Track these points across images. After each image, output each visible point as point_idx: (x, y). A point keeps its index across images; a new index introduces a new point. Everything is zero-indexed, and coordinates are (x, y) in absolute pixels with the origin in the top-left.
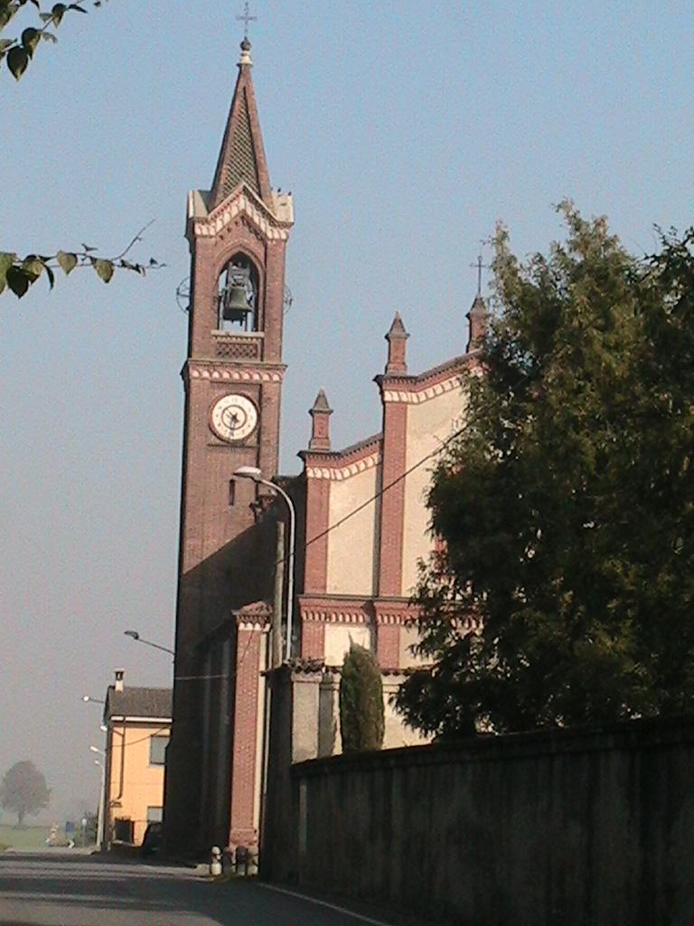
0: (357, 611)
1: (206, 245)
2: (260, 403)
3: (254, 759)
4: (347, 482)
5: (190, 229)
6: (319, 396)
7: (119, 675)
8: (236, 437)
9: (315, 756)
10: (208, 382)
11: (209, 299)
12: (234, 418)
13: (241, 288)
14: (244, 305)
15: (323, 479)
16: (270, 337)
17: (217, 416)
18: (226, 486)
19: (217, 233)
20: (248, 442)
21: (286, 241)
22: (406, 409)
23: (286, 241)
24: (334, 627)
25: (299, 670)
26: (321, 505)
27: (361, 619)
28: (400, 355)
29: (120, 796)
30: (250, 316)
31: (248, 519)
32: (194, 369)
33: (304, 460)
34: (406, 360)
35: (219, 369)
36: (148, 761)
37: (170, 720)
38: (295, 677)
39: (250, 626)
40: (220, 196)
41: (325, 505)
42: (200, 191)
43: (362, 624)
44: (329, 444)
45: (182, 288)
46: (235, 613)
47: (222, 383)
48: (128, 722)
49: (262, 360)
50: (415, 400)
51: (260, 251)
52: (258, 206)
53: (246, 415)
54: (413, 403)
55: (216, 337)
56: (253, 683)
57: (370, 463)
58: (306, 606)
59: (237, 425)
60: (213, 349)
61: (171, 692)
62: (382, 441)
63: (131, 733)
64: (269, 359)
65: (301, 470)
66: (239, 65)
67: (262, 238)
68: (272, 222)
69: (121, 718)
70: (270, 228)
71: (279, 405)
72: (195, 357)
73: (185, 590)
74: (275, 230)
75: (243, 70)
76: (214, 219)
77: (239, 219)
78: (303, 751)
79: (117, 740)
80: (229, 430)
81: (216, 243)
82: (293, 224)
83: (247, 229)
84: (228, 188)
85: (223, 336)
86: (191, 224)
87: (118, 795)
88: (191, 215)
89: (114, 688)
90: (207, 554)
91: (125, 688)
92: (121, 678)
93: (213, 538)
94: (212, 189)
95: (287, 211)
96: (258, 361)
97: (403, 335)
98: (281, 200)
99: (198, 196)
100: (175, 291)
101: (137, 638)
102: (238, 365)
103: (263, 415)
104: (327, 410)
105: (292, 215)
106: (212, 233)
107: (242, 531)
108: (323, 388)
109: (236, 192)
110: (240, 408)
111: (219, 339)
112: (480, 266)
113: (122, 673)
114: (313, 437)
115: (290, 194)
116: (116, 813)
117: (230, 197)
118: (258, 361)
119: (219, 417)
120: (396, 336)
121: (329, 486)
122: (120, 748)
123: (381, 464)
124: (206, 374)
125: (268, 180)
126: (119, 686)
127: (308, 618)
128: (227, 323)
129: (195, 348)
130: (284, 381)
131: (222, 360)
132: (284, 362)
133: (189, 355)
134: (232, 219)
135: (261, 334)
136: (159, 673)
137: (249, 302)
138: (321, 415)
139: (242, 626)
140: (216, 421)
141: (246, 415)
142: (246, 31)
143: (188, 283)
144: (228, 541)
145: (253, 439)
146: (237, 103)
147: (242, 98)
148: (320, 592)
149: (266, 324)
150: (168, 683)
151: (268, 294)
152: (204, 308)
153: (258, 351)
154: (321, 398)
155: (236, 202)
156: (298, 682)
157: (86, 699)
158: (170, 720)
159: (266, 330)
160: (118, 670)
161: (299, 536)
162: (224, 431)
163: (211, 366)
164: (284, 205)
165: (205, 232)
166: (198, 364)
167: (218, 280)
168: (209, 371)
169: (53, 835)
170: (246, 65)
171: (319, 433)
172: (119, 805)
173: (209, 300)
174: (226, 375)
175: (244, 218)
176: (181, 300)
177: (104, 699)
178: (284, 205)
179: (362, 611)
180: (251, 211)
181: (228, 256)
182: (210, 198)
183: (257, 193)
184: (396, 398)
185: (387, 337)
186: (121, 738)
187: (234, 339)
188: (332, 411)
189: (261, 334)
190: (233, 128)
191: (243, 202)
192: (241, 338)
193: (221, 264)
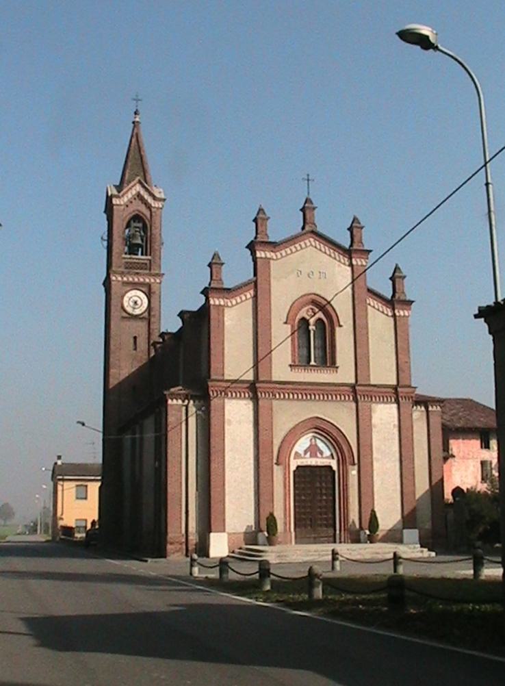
0: (244, 390)
2: (150, 294)
4: (279, 261)
5: (109, 202)
6: (215, 255)
10: (120, 283)
12: (136, 303)
18: (132, 341)
21: (161, 208)
22: (269, 263)
24: (230, 401)
26: (219, 321)
27: (247, 395)
29: (62, 514)
34: (268, 232)
36: (74, 498)
39: (175, 401)
40: (125, 185)
41: (221, 321)
42: (114, 186)
43: (247, 398)
44: (223, 284)
46: (165, 392)
47: (128, 283)
49: (150, 270)
50: (275, 258)
51: (147, 213)
52: (147, 190)
57: (249, 296)
58: (212, 387)
59: (137, 307)
60: (123, 266)
62: (256, 283)
63: (66, 484)
64: (154, 269)
65: (203, 302)
66: (134, 122)
67: (149, 207)
68: (154, 198)
69: (61, 477)
77: (136, 197)
79: (60, 488)
81: (124, 209)
83: (140, 202)
86: (109, 199)
88: (110, 194)
89: (56, 463)
90: (122, 378)
93: (124, 369)
96: (147, 272)
101: (83, 424)
102: (137, 273)
106: (122, 203)
107: (140, 365)
110: (139, 297)
112: (308, 180)
116: (61, 523)
120: (259, 220)
121: (223, 310)
123: (255, 297)
124: (120, 279)
126: (59, 462)
127: (213, 394)
130: (162, 283)
132: (162, 272)
134: (129, 200)
135: (149, 257)
138: (217, 265)
139: (170, 402)
140: (126, 304)
142: (137, 106)
144: (133, 370)
145: (146, 315)
147: (135, 137)
148: (221, 378)
152: (118, 245)
154: (216, 256)
155: (134, 188)
157: (44, 469)
162: (129, 310)
163: (122, 274)
165: (118, 203)
170: (138, 122)
172: (62, 519)
173: (121, 240)
174: (131, 279)
175: (139, 195)
177: (52, 469)
179: (247, 390)
180: (143, 192)
182: (119, 188)
183: (144, 183)
184: (263, 256)
188: (269, 218)
189: (149, 257)
191: (138, 188)
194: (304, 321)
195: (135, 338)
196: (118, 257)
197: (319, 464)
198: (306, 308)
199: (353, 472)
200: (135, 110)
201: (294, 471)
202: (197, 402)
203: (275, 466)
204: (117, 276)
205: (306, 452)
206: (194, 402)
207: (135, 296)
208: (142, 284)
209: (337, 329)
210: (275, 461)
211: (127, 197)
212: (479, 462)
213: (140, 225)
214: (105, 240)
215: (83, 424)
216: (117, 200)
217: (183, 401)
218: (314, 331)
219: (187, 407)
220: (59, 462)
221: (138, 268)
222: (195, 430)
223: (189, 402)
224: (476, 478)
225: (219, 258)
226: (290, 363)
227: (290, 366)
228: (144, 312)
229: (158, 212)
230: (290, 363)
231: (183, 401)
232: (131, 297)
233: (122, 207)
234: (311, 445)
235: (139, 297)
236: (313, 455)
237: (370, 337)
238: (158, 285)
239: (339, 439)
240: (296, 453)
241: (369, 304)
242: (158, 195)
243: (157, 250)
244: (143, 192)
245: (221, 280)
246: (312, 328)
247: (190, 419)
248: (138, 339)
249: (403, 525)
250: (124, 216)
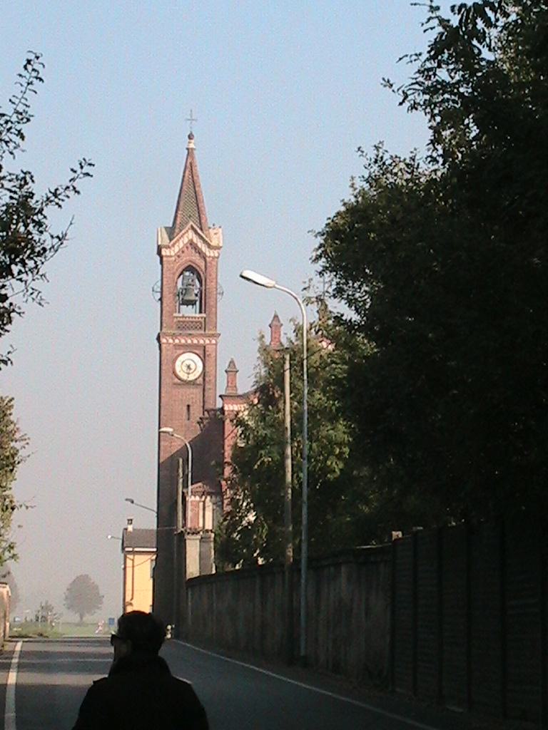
1: (169, 261)
2: (205, 357)
6: (231, 362)
7: (130, 521)
8: (189, 379)
9: (198, 575)
10: (171, 346)
11: (171, 295)
12: (189, 367)
13: (191, 287)
14: (193, 297)
16: (209, 317)
18: (185, 408)
19: (175, 254)
20: (198, 382)
21: (218, 258)
23: (218, 258)
25: (189, 533)
28: (278, 337)
29: (132, 599)
30: (198, 303)
31: (197, 431)
32: (163, 337)
33: (222, 399)
35: (179, 337)
38: (187, 537)
40: (177, 231)
45: (155, 287)
48: (137, 552)
49: (205, 330)
51: (202, 264)
52: (201, 237)
53: (196, 364)
55: (177, 317)
59: (192, 371)
60: (175, 326)
61: (155, 532)
64: (210, 330)
66: (188, 149)
67: (204, 258)
68: (209, 246)
69: (131, 549)
70: (207, 249)
71: (216, 360)
72: (164, 330)
74: (211, 251)
75: (190, 152)
76: (173, 245)
77: (188, 245)
78: (192, 573)
79: (129, 563)
80: (186, 375)
81: (175, 261)
82: (221, 247)
83: (193, 251)
84: (182, 226)
85: (180, 317)
87: (130, 597)
89: (126, 529)
91: (134, 529)
92: (131, 523)
94: (173, 225)
95: (219, 238)
97: (279, 324)
98: (215, 231)
99: (164, 230)
100: (151, 290)
101: (132, 502)
103: (206, 365)
104: (235, 370)
105: (221, 242)
106: (173, 254)
108: (232, 357)
109: (187, 229)
110: (193, 361)
111: (179, 319)
113: (131, 520)
114: (228, 386)
115: (220, 227)
117: (183, 232)
118: (203, 332)
122: (131, 569)
124: (171, 341)
125: (206, 220)
126: (130, 528)
128: (183, 307)
129: (164, 325)
131: (181, 332)
133: (161, 330)
135: (204, 315)
136: (148, 521)
137: (196, 295)
140: (178, 369)
141: (196, 364)
143: (159, 284)
145: (201, 379)
146: (187, 172)
147: (190, 168)
149: (207, 309)
150: (154, 527)
151: (207, 290)
153: (202, 326)
155: (187, 234)
156: (189, 539)
157: (109, 537)
158: (155, 550)
159: (207, 312)
160: (129, 518)
162: (184, 376)
163: (174, 336)
164: (216, 234)
165: (168, 254)
166: (166, 335)
167: (176, 283)
168: (172, 338)
169: (100, 628)
170: (192, 149)
171: (231, 383)
172: (131, 604)
174: (183, 341)
175: (191, 243)
176: (155, 294)
177: (121, 537)
178: (216, 234)
180: (196, 240)
181: (183, 267)
182: (171, 232)
183: (201, 226)
185: (270, 326)
186: (131, 562)
187: (187, 319)
190: (184, 188)
191: (191, 235)
192: (192, 318)
193: (180, 270)
195: (188, 406)
196: (169, 316)
200: (189, 133)
202: (214, 498)
204: (168, 338)
206: (211, 497)
207: (189, 359)
208: (197, 346)
211: (178, 246)
214: (157, 292)
215: (132, 502)
216: (168, 251)
217: (201, 497)
219: (204, 502)
220: (130, 528)
222: (211, 518)
223: (206, 498)
225: (234, 365)
228: (199, 377)
229: (214, 263)
231: (201, 497)
232: (184, 362)
233: (173, 259)
235: (193, 361)
238: (214, 346)
242: (214, 243)
243: (212, 306)
244: (196, 240)
245: (235, 386)
247: (207, 509)
248: (191, 408)
250: (176, 268)
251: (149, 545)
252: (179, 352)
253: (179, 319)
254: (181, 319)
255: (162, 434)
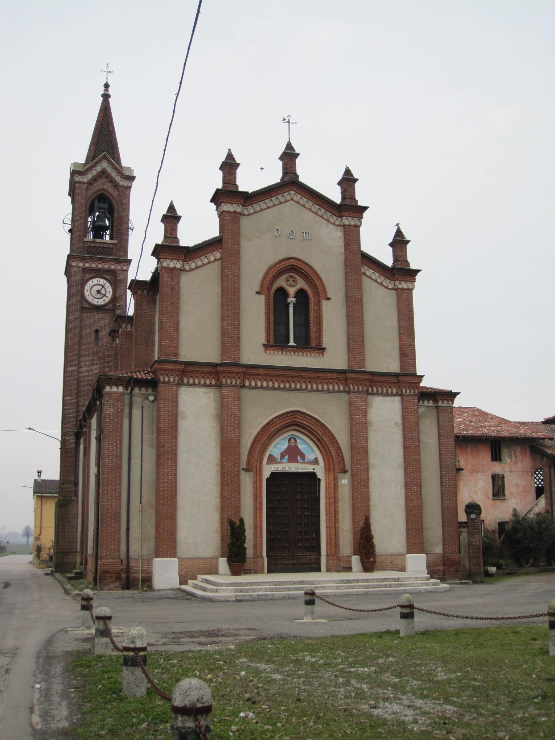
3: (120, 497)
15: (175, 268)
17: (87, 290)
18: (93, 334)
37: (57, 495)
54: (244, 215)
56: (117, 435)
73: (68, 399)
119: (89, 292)
135: (115, 242)
147: (106, 97)
158: (57, 495)
161: (104, 502)
175: (103, 173)
181: (95, 196)
189: (115, 242)
194: (282, 293)
197: (300, 471)
198: (286, 276)
199: (344, 481)
201: (267, 480)
203: (243, 474)
205: (282, 456)
209: (324, 302)
210: (244, 465)
212: (490, 476)
213: (106, 206)
218: (294, 304)
221: (98, 253)
224: (486, 493)
226: (264, 342)
227: (264, 345)
230: (264, 342)
234: (289, 446)
236: (292, 460)
237: (354, 578)
239: (325, 439)
240: (270, 455)
241: (364, 274)
244: (109, 170)
246: (292, 300)
249: (408, 549)
251: (52, 491)
252: (88, 276)
253: (89, 244)
254: (92, 245)
255: (77, 185)
